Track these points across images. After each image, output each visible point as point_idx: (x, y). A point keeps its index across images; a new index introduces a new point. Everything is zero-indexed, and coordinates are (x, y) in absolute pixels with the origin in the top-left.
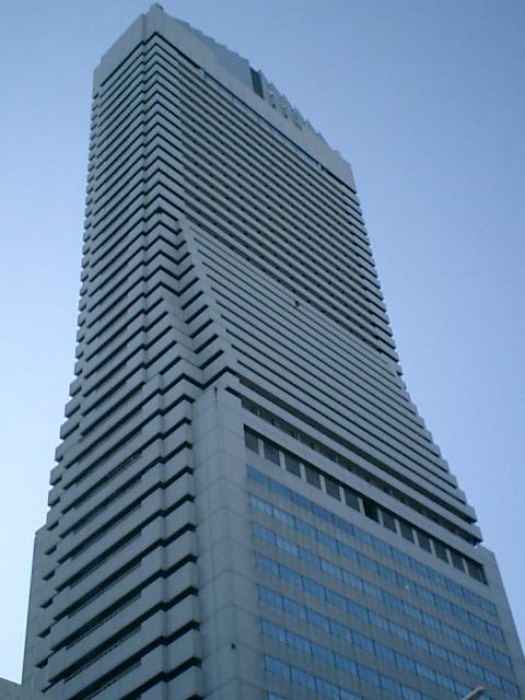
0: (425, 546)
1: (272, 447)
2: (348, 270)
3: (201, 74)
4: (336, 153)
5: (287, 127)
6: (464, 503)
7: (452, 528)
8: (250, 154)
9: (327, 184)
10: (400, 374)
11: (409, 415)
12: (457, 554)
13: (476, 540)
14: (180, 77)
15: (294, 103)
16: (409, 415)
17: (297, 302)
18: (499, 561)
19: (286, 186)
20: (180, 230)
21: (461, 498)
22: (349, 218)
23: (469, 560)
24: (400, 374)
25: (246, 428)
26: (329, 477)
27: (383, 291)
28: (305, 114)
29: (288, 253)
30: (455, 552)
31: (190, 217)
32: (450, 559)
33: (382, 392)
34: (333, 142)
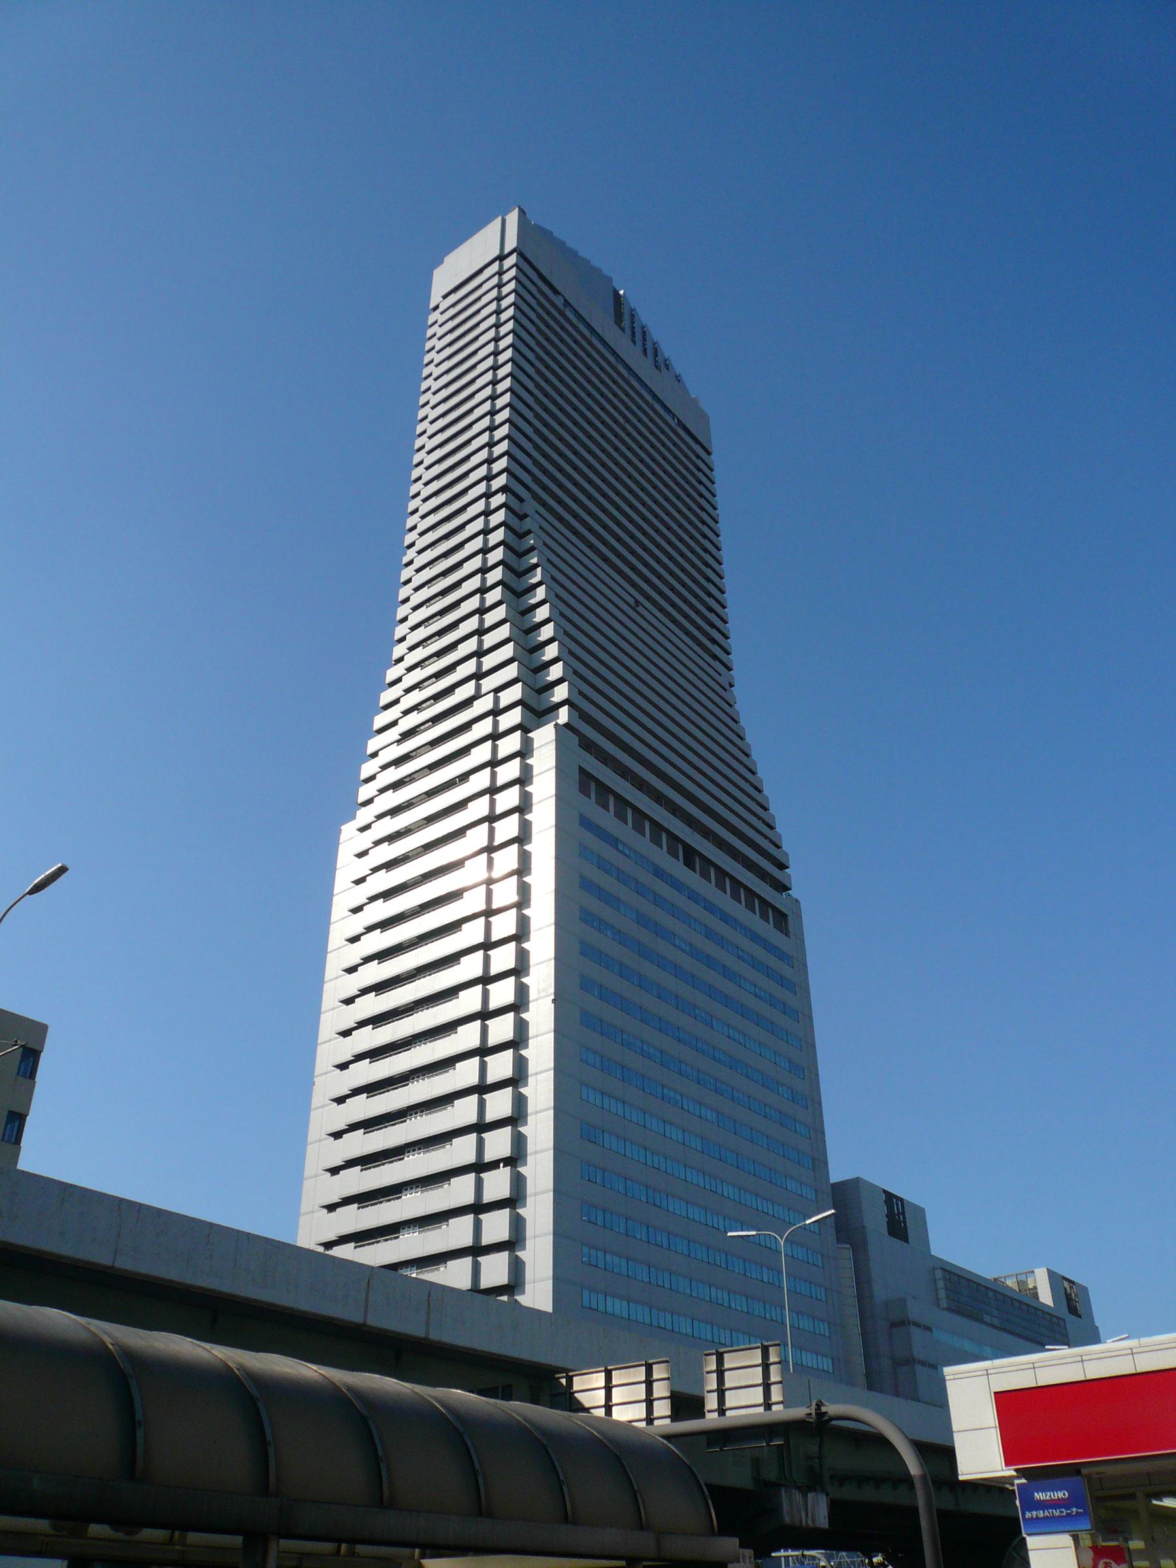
0: (656, 840)
1: (604, 790)
2: (662, 449)
3: (559, 302)
4: (695, 402)
5: (643, 366)
6: (779, 847)
7: (763, 875)
8: (589, 395)
9: (682, 445)
10: (731, 686)
11: (726, 707)
12: (765, 903)
13: (782, 888)
14: (539, 323)
15: (655, 334)
16: (726, 707)
17: (637, 601)
18: (720, 460)
19: (650, 502)
20: (526, 516)
21: (752, 767)
22: (700, 475)
23: (776, 910)
24: (731, 686)
25: (582, 770)
26: (619, 798)
27: (724, 555)
28: (667, 350)
29: (590, 452)
30: (763, 902)
31: (535, 497)
32: (612, 808)
33: (712, 713)
34: (696, 386)
